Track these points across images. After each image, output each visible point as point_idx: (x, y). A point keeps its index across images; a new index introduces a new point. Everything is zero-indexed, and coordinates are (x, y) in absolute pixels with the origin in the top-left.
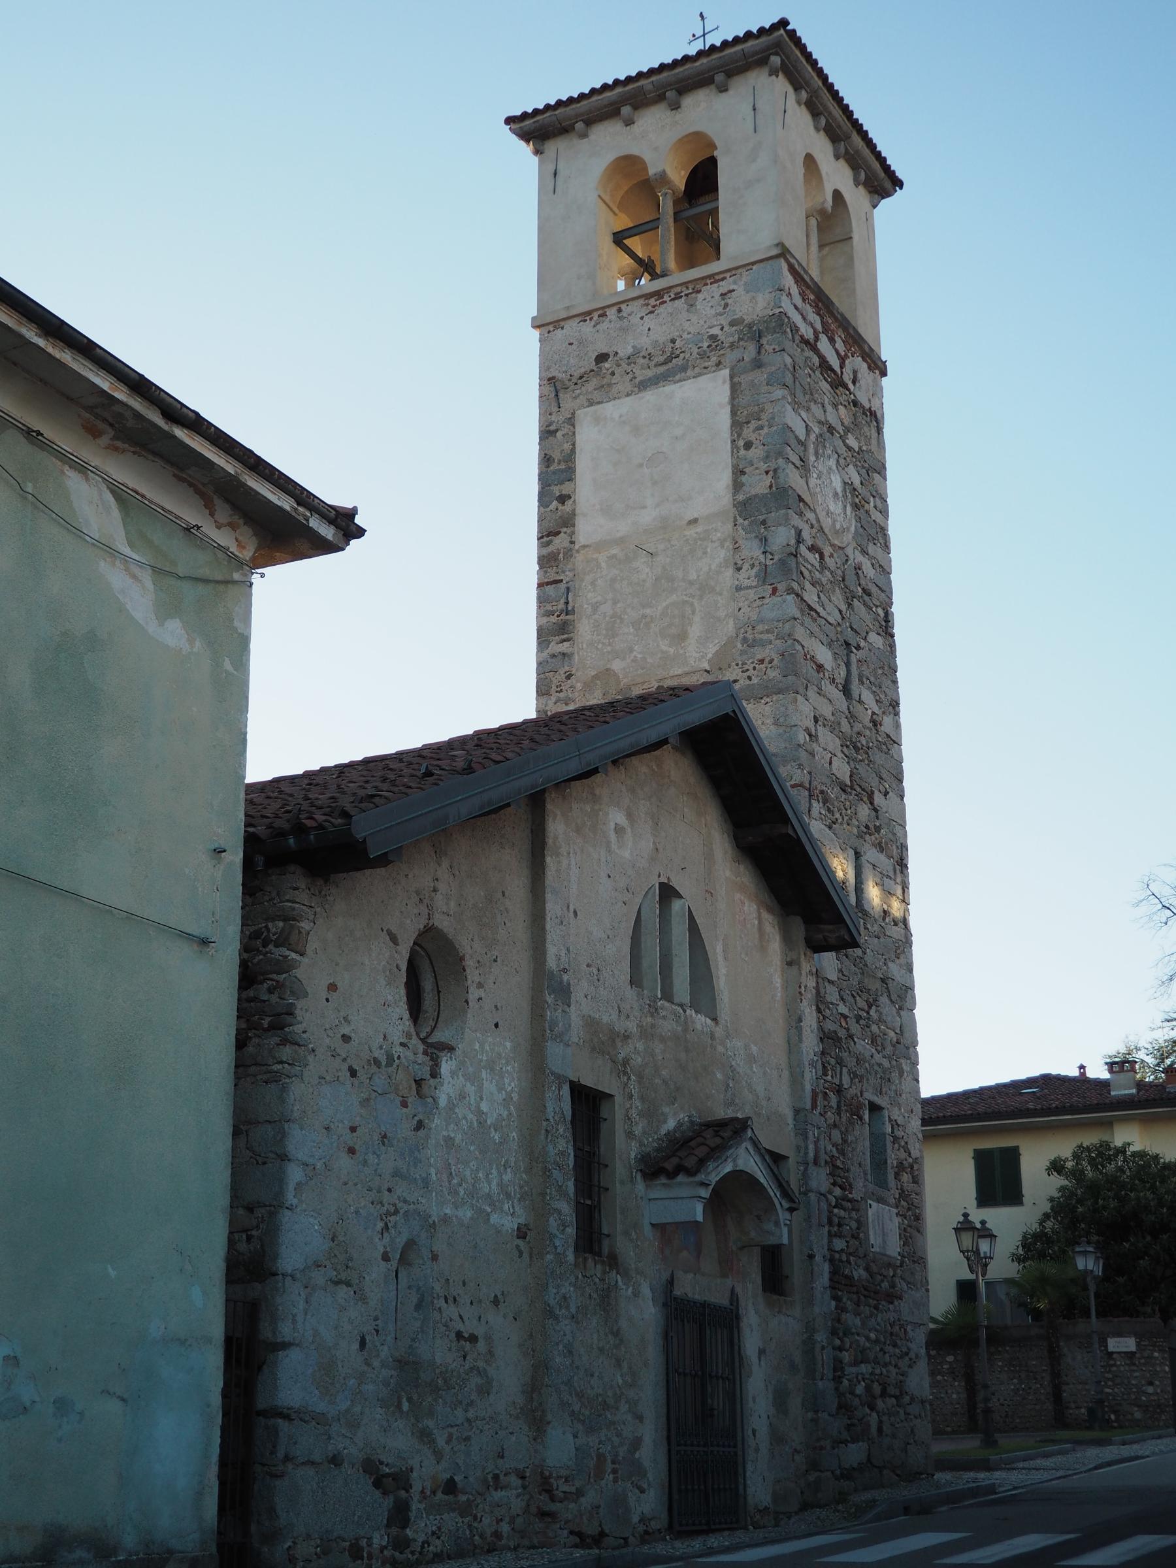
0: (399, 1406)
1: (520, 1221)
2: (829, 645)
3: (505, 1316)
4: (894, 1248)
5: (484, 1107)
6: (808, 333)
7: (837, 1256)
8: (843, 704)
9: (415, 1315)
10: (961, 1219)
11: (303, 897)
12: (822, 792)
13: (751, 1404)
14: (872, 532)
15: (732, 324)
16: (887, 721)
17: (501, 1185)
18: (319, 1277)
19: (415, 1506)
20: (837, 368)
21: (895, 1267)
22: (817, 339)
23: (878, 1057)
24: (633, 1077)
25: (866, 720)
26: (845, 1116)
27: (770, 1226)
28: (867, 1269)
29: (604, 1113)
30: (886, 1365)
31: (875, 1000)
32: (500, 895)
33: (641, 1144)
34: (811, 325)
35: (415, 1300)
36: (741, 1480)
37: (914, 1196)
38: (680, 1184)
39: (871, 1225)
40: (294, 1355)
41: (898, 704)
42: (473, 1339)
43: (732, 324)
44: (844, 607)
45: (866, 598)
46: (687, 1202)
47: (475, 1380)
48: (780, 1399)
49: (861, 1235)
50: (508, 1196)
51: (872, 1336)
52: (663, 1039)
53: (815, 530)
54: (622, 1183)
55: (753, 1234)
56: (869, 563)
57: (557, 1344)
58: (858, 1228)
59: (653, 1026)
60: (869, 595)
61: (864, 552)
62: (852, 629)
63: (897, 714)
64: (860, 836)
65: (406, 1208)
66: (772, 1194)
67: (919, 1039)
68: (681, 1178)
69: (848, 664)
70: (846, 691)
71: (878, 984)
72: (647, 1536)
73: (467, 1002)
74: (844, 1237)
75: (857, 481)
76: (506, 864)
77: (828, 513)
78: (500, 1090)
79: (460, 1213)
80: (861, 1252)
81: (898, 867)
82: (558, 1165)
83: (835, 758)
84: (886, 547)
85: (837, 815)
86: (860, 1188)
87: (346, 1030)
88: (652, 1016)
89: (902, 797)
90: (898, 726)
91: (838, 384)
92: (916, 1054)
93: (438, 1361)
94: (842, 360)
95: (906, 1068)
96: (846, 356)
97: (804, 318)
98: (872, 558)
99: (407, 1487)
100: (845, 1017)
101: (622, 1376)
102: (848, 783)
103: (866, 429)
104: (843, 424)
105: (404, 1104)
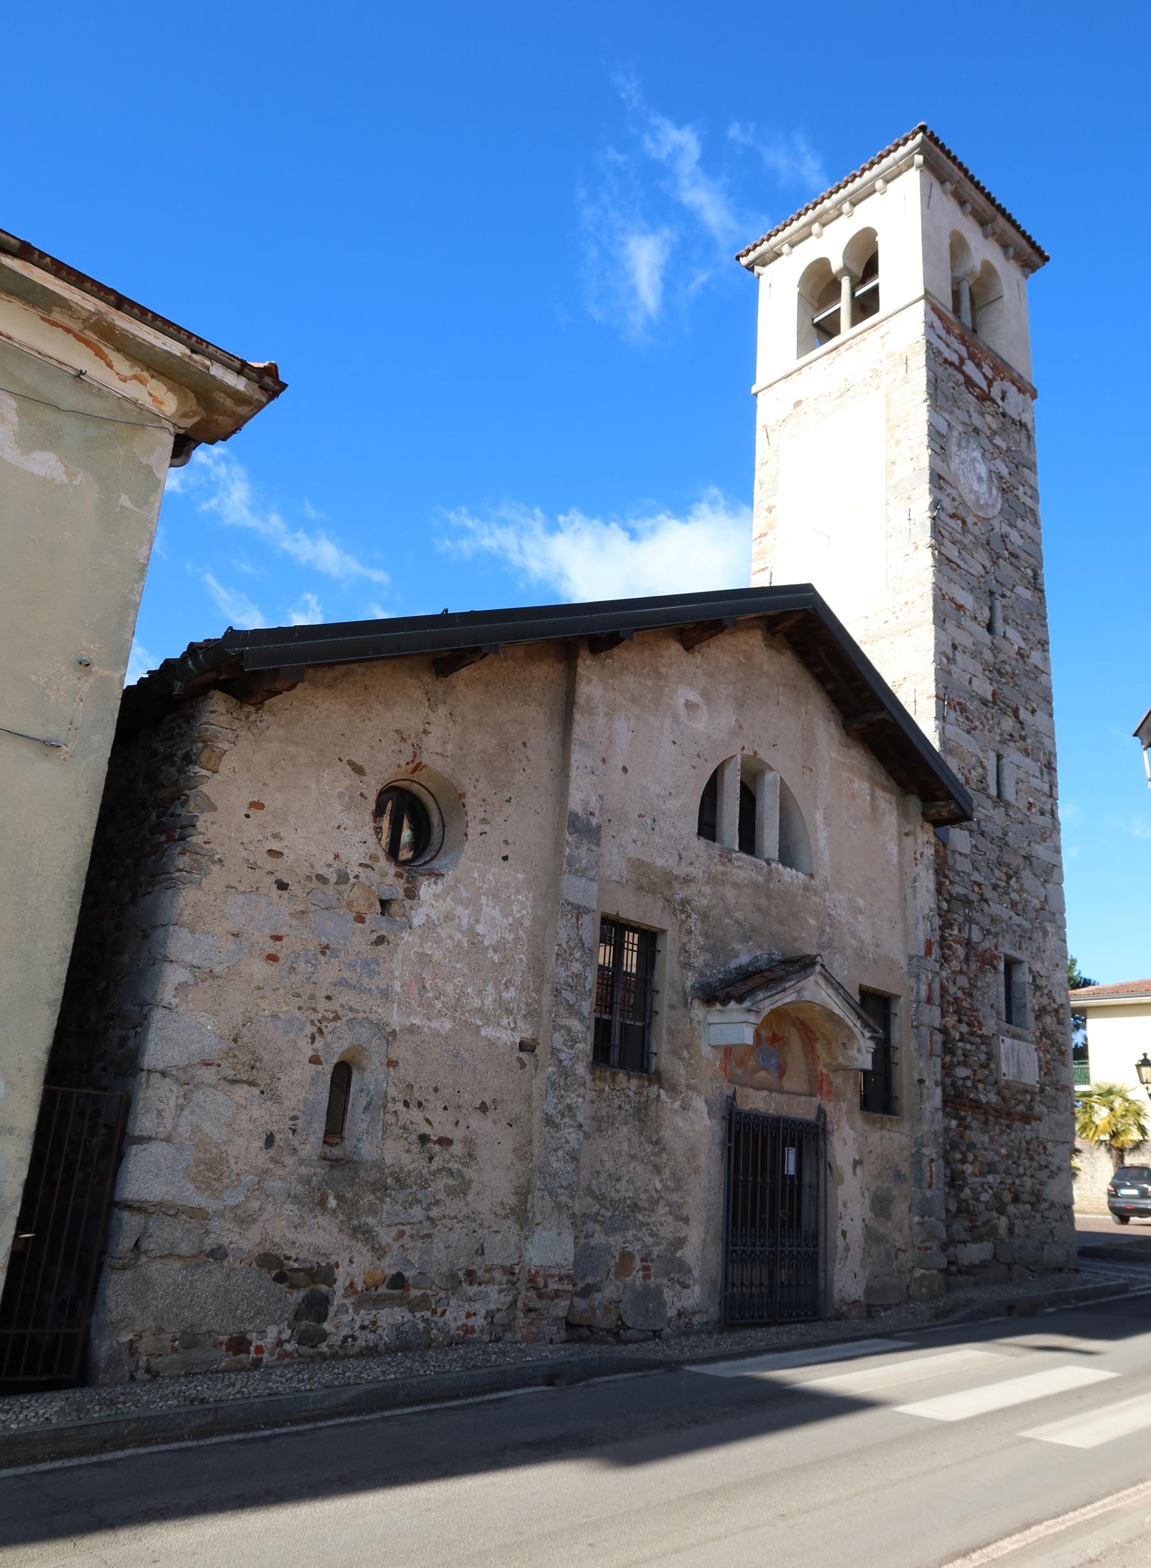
0: (323, 1203)
1: (523, 1035)
2: (971, 590)
3: (494, 1122)
4: (1031, 1077)
5: (480, 929)
6: (955, 359)
7: (960, 1082)
8: (986, 638)
9: (363, 1116)
10: (1142, 1058)
11: (224, 719)
12: (960, 704)
13: (841, 1208)
14: (1022, 511)
15: (888, 357)
16: (1035, 657)
17: (499, 1001)
18: (208, 1075)
19: (337, 1300)
20: (986, 389)
21: (1033, 1094)
22: (962, 361)
23: (1017, 919)
24: (694, 916)
25: (1013, 653)
26: (974, 966)
27: (854, 1053)
28: (999, 1093)
29: (659, 946)
30: (1020, 1176)
31: (1016, 873)
32: (519, 744)
33: (702, 974)
34: (956, 352)
35: (364, 1103)
36: (822, 1275)
37: (1058, 1035)
38: (731, 1010)
39: (1003, 1058)
40: (156, 1149)
41: (1047, 643)
42: (445, 1142)
43: (888, 357)
44: (988, 564)
45: (1012, 559)
46: (736, 1026)
47: (444, 1181)
48: (881, 1205)
49: (993, 1066)
50: (509, 1012)
51: (1004, 1151)
52: (735, 885)
53: (956, 503)
54: (673, 1007)
55: (841, 1059)
56: (1017, 535)
57: (556, 1150)
58: (988, 1059)
59: (724, 874)
60: (1017, 557)
61: (1012, 525)
62: (997, 581)
63: (1045, 651)
64: (1003, 742)
65: (351, 1015)
66: (851, 1024)
67: (1067, 907)
68: (732, 1005)
69: (991, 609)
70: (990, 628)
71: (1020, 861)
72: (687, 1331)
73: (466, 835)
74: (970, 1066)
75: (1005, 471)
76: (530, 718)
77: (971, 490)
78: (505, 915)
79: (435, 1024)
80: (991, 1080)
81: (1045, 770)
82: (569, 985)
83: (974, 679)
84: (1036, 523)
85: (977, 723)
86: (990, 1025)
87: (276, 846)
88: (724, 864)
89: (1051, 716)
90: (1046, 660)
91: (984, 398)
92: (1064, 920)
93: (389, 1160)
94: (990, 383)
95: (1050, 928)
96: (994, 379)
97: (948, 346)
98: (1019, 530)
99: (331, 1280)
100: (979, 885)
101: (661, 1181)
102: (990, 698)
103: (1016, 435)
104: (990, 428)
105: (360, 919)
